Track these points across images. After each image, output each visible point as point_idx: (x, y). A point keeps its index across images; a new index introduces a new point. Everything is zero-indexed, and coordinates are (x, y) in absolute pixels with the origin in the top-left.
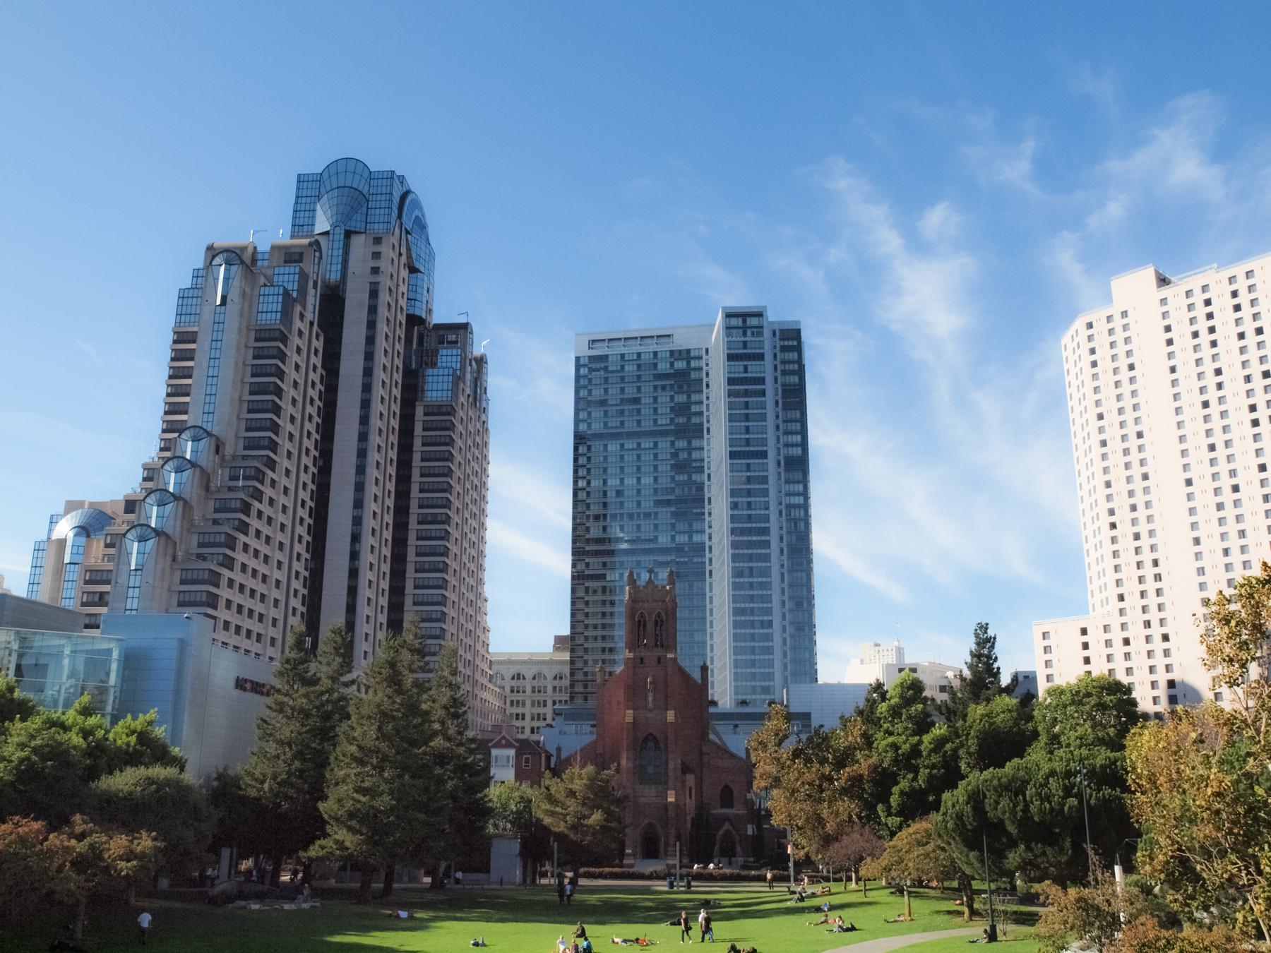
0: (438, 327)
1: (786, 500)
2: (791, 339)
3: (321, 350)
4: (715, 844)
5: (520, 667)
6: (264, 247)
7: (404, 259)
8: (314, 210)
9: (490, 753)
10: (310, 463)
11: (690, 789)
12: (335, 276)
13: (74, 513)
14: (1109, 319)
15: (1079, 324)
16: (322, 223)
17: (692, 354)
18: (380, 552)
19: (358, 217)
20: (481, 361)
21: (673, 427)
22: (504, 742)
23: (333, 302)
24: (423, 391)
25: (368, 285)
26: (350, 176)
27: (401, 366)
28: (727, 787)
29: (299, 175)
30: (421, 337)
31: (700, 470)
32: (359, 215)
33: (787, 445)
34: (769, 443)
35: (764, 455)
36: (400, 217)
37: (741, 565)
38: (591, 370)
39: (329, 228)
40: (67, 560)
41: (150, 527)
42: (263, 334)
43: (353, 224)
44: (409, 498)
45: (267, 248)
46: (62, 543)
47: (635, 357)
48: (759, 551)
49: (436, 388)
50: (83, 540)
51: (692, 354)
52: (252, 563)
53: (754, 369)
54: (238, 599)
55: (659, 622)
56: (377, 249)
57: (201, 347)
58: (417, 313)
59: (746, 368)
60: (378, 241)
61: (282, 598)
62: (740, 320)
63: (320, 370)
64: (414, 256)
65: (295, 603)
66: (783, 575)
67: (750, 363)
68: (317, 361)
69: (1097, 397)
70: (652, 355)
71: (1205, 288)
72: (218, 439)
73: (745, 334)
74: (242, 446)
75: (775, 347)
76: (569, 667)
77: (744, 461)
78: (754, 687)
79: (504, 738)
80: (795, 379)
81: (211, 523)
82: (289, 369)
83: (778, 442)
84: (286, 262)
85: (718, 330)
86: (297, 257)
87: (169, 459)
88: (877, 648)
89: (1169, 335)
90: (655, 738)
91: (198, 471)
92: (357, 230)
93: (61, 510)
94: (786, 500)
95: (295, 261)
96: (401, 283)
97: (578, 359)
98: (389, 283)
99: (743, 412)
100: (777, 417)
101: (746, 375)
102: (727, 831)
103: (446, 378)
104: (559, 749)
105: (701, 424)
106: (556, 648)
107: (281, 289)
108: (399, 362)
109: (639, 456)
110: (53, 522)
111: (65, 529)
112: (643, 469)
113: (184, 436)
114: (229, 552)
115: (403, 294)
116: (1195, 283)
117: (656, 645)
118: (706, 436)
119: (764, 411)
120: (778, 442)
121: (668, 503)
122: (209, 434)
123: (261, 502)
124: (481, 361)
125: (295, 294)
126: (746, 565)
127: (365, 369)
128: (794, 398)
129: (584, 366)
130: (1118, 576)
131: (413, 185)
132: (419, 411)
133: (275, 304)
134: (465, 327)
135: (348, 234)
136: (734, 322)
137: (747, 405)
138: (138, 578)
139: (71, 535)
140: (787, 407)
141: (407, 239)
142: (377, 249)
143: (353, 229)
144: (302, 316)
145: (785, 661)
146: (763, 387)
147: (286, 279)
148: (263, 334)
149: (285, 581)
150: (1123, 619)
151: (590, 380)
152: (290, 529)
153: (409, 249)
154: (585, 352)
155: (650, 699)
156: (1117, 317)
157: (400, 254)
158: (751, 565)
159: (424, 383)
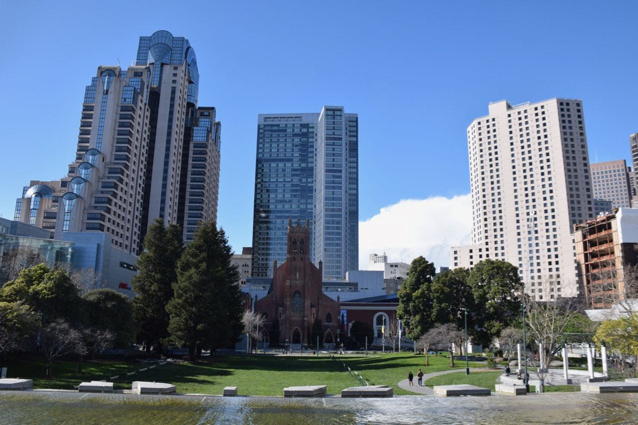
0: (200, 108)
1: (349, 191)
2: (353, 122)
3: (149, 116)
4: (323, 338)
5: (246, 261)
6: (124, 68)
7: (187, 77)
8: (148, 53)
13: (35, 186)
14: (488, 121)
15: (475, 122)
16: (151, 59)
17: (310, 125)
18: (173, 208)
19: (167, 57)
20: (219, 124)
23: (155, 97)
24: (193, 136)
26: (164, 38)
27: (184, 125)
28: (329, 313)
29: (141, 37)
30: (192, 113)
35: (340, 188)
36: (186, 58)
38: (265, 131)
39: (153, 62)
40: (32, 207)
41: (73, 193)
42: (124, 109)
44: (186, 184)
45: (126, 69)
46: (29, 199)
47: (284, 126)
48: (337, 213)
49: (199, 135)
50: (38, 199)
52: (119, 211)
54: (112, 227)
55: (302, 242)
56: (175, 72)
57: (96, 113)
60: (176, 68)
61: (130, 227)
62: (332, 112)
63: (148, 126)
64: (191, 76)
65: (136, 230)
66: (346, 224)
68: (147, 121)
69: (482, 159)
70: (292, 125)
71: (525, 111)
73: (334, 118)
74: (114, 158)
76: (251, 261)
78: (333, 272)
81: (100, 192)
82: (135, 124)
83: (347, 166)
84: (135, 76)
85: (322, 117)
86: (140, 74)
87: (81, 164)
88: (376, 257)
89: (514, 170)
91: (95, 169)
93: (29, 185)
94: (349, 191)
95: (139, 76)
97: (259, 126)
98: (181, 88)
102: (329, 332)
103: (204, 131)
104: (256, 296)
106: (244, 253)
107: (133, 88)
108: (183, 123)
110: (25, 190)
111: (31, 193)
112: (286, 175)
113: (88, 153)
116: (522, 109)
120: (347, 166)
124: (219, 124)
125: (139, 91)
126: (331, 219)
128: (353, 149)
129: (262, 129)
130: (486, 228)
131: (192, 44)
132: (191, 146)
133: (130, 95)
134: (213, 109)
135: (162, 65)
136: (329, 113)
137: (334, 144)
138: (69, 217)
139: (34, 196)
141: (188, 69)
142: (175, 72)
143: (165, 62)
144: (142, 101)
147: (135, 84)
148: (124, 109)
149: (133, 203)
150: (487, 247)
151: (264, 135)
153: (189, 73)
154: (263, 122)
155: (298, 275)
156: (491, 120)
157: (185, 75)
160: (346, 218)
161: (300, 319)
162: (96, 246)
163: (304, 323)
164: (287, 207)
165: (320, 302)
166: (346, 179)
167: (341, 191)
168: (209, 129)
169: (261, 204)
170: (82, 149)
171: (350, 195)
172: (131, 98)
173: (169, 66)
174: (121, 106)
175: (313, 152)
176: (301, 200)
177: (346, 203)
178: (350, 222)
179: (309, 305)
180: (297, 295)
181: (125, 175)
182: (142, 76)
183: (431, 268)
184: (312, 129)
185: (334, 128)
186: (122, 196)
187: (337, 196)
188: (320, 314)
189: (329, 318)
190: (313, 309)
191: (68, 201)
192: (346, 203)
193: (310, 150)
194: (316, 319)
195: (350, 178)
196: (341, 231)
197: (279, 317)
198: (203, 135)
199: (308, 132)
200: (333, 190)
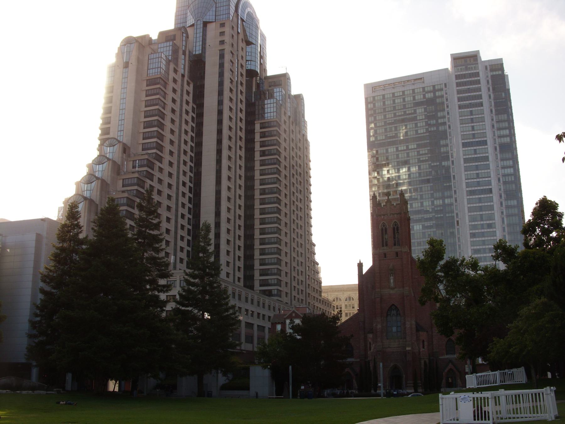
1: (501, 172)
11: (423, 341)
12: (198, 51)
17: (436, 88)
19: (211, 13)
21: (428, 134)
22: (294, 315)
25: (218, 51)
31: (447, 158)
32: (211, 12)
33: (500, 137)
34: (488, 136)
35: (485, 143)
43: (208, 17)
47: (401, 94)
58: (253, 68)
60: (223, 25)
63: (191, 104)
64: (248, 34)
66: (503, 219)
75: (487, 77)
77: (472, 148)
83: (494, 136)
90: (396, 307)
92: (211, 20)
100: (492, 120)
102: (451, 369)
105: (448, 152)
109: (408, 154)
114: (279, 288)
115: (242, 57)
117: (395, 245)
118: (449, 137)
119: (483, 116)
120: (494, 136)
121: (428, 181)
122: (119, 142)
123: (152, 181)
127: (219, 101)
132: (257, 127)
135: (205, 24)
137: (471, 113)
140: (498, 113)
143: (208, 20)
146: (481, 100)
152: (233, 232)
155: (392, 281)
158: (481, 213)
159: (263, 109)
164: (413, 155)
166: (496, 155)
173: (215, 23)
174: (147, 80)
179: (414, 326)
180: (394, 312)
181: (156, 168)
182: (174, 39)
184: (440, 92)
185: (478, 176)
192: (500, 189)
197: (368, 349)
198: (269, 105)
199: (435, 97)
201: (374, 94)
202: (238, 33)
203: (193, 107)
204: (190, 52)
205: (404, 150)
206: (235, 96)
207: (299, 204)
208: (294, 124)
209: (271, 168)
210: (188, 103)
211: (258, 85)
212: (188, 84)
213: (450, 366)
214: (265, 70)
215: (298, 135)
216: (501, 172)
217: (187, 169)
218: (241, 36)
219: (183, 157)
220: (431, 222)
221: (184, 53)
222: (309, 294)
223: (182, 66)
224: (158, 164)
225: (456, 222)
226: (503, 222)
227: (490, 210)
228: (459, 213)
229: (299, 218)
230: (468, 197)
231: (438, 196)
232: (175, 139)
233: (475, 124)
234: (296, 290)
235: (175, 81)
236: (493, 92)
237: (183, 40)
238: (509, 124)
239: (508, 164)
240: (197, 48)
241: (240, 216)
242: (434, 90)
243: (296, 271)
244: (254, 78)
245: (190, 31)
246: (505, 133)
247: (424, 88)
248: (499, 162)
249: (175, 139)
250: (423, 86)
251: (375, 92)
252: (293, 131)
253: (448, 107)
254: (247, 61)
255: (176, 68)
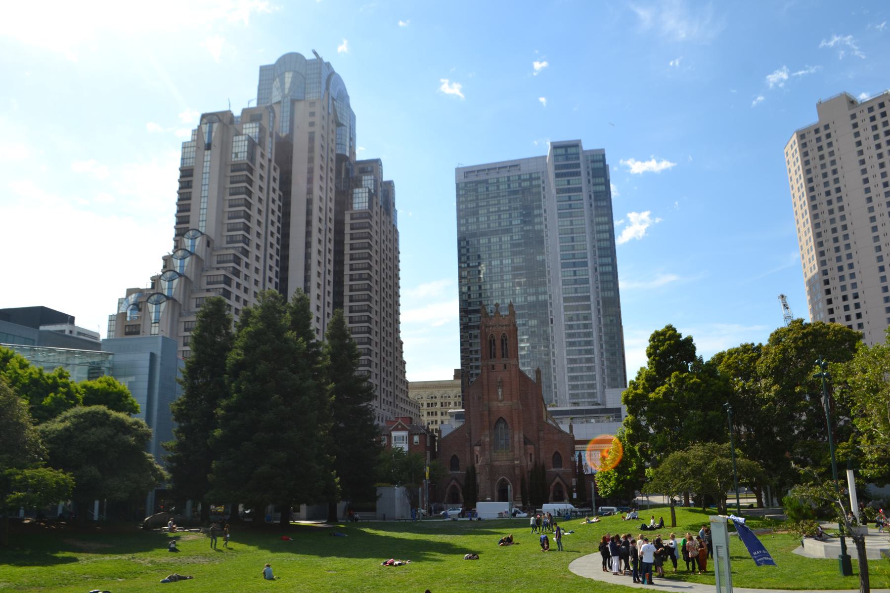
1: (596, 228)
9: (391, 434)
10: (275, 220)
11: (531, 454)
12: (284, 134)
17: (533, 176)
22: (400, 427)
28: (557, 453)
35: (585, 264)
36: (327, 88)
37: (571, 313)
39: (280, 99)
51: (533, 176)
53: (574, 182)
59: (569, 181)
63: (278, 192)
64: (339, 115)
66: (599, 319)
67: (571, 178)
72: (208, 236)
79: (400, 424)
80: (603, 188)
90: (504, 420)
91: (194, 257)
96: (330, 132)
99: (570, 244)
101: (569, 186)
106: (456, 377)
115: (332, 140)
126: (574, 312)
136: (560, 151)
137: (570, 198)
138: (157, 328)
144: (262, 155)
145: (599, 307)
155: (500, 393)
157: (329, 113)
158: (577, 312)
160: (599, 310)
161: (508, 463)
162: (148, 356)
163: (514, 469)
165: (541, 434)
167: (587, 268)
168: (373, 191)
169: (469, 301)
170: (180, 233)
171: (602, 274)
172: (244, 152)
175: (541, 223)
176: (528, 290)
177: (597, 288)
178: (605, 316)
180: (502, 425)
181: (243, 264)
182: (261, 119)
183: (686, 347)
185: (570, 207)
186: (239, 294)
187: (581, 277)
188: (542, 455)
189: (557, 459)
190: (529, 446)
191: (154, 306)
192: (597, 288)
193: (536, 212)
194: (536, 462)
195: (600, 249)
196: (591, 330)
199: (531, 186)
200: (575, 269)
201: (466, 180)
202: (329, 113)
203: (279, 195)
204: (276, 133)
205: (495, 212)
206: (326, 154)
207: (388, 252)
208: (385, 215)
209: (362, 253)
210: (274, 190)
211: (347, 170)
212: (275, 169)
213: (558, 480)
214: (354, 153)
215: (389, 226)
216: (596, 228)
217: (273, 263)
218: (332, 117)
219: (271, 217)
220: (524, 319)
221: (271, 136)
222: (397, 395)
223: (269, 150)
224: (244, 259)
225: (549, 304)
226: (600, 323)
227: (593, 380)
228: (556, 361)
229: (389, 305)
230: (568, 349)
231: (531, 291)
232: (264, 196)
233: (574, 218)
234: (385, 392)
235: (262, 166)
236: (603, 307)
237: (270, 121)
238: (606, 186)
239: (605, 237)
240: (284, 129)
241: (329, 282)
242: (531, 179)
243: (385, 341)
244: (344, 164)
245: (277, 109)
246: (607, 261)
247: (519, 176)
248: (597, 259)
249: (264, 196)
250: (519, 174)
251: (467, 177)
252: (384, 222)
253: (544, 197)
254: (337, 144)
255: (264, 153)
